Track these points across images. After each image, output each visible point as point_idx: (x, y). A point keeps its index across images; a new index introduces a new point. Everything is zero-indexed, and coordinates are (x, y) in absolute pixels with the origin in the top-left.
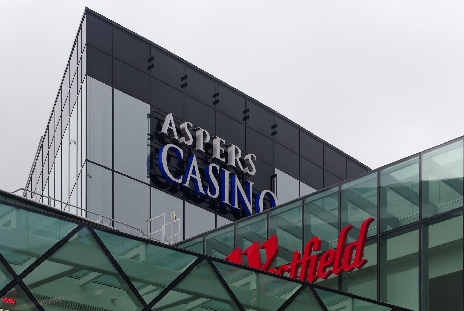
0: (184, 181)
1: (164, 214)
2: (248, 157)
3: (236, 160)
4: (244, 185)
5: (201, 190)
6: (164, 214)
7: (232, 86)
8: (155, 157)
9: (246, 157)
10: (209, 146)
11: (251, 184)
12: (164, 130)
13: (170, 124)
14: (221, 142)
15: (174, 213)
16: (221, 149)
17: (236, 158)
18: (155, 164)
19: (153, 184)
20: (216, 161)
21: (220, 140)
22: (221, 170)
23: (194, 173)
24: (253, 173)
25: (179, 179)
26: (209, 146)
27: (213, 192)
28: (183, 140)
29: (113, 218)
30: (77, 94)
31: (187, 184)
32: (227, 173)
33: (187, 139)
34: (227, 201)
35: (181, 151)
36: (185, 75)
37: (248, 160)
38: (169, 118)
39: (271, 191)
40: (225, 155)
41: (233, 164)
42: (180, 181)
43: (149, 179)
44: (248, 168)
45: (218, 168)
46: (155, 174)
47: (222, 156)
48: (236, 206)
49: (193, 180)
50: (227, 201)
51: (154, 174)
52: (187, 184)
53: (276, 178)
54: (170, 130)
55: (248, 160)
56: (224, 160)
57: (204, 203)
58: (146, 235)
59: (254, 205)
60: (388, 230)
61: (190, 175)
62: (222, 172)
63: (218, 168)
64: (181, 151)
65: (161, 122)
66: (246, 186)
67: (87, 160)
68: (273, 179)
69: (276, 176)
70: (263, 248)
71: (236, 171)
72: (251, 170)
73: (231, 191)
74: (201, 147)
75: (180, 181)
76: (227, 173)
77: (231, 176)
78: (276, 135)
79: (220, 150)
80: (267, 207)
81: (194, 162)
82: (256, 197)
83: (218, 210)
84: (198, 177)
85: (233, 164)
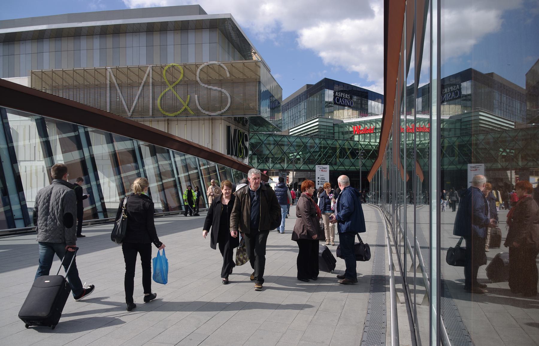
2: (348, 95)
10: (342, 96)
12: (336, 95)
38: (337, 93)
49: (340, 102)
66: (348, 101)
77: (346, 100)
82: (350, 102)
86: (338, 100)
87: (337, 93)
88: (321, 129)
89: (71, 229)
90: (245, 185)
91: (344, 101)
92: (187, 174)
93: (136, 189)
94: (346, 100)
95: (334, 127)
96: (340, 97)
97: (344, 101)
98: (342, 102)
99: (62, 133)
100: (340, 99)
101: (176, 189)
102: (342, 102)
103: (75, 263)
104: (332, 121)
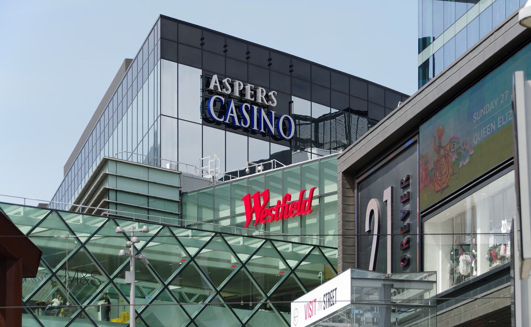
0: (225, 119)
1: (209, 157)
2: (271, 93)
3: (262, 98)
4: (269, 116)
5: (237, 123)
6: (209, 157)
7: (259, 44)
8: (206, 105)
9: (269, 94)
10: (242, 93)
11: (273, 112)
12: (212, 87)
13: (216, 82)
14: (251, 87)
15: (216, 155)
16: (251, 92)
17: (262, 96)
18: (205, 109)
19: (205, 122)
20: (247, 101)
21: (251, 86)
22: (251, 107)
23: (232, 112)
24: (275, 105)
25: (222, 118)
26: (242, 93)
27: (245, 123)
28: (224, 91)
29: (178, 161)
30: (154, 66)
31: (227, 121)
32: (256, 108)
33: (227, 90)
34: (255, 128)
35: (223, 99)
36: (226, 44)
37: (271, 95)
38: (215, 78)
39: (289, 115)
40: (254, 95)
41: (260, 101)
42: (222, 120)
43: (201, 119)
44: (271, 102)
45: (249, 106)
46: (206, 117)
47: (252, 97)
48: (262, 130)
49: (233, 118)
50: (255, 128)
51: (204, 117)
52: (227, 121)
53: (292, 104)
54: (216, 87)
55: (271, 95)
56: (253, 99)
57: (240, 129)
58: (198, 169)
59: (276, 128)
60: (325, 193)
61: (229, 114)
62: (252, 108)
63: (249, 106)
64: (223, 99)
65: (210, 79)
66: (269, 114)
67: (161, 115)
68: (290, 104)
69: (292, 102)
70: (262, 195)
71: (261, 106)
72: (273, 102)
73: (258, 117)
74: (237, 94)
75: (222, 120)
76: (256, 108)
77: (259, 112)
78: (292, 73)
79: (251, 93)
80: (287, 126)
81: (232, 105)
82: (277, 118)
83: (251, 132)
84: (235, 115)
85: (260, 101)
86: (223, 111)
87: (215, 78)
88: (151, 200)
89: (36, 278)
90: (108, 295)
91: (250, 112)
92: (67, 250)
93: (236, 265)
94: (259, 112)
95: (181, 204)
96: (229, 97)
97: (250, 112)
98: (241, 117)
99: (491, 270)
100: (229, 104)
101: (412, 281)
102: (241, 117)
103: (445, 295)
104: (175, 181)
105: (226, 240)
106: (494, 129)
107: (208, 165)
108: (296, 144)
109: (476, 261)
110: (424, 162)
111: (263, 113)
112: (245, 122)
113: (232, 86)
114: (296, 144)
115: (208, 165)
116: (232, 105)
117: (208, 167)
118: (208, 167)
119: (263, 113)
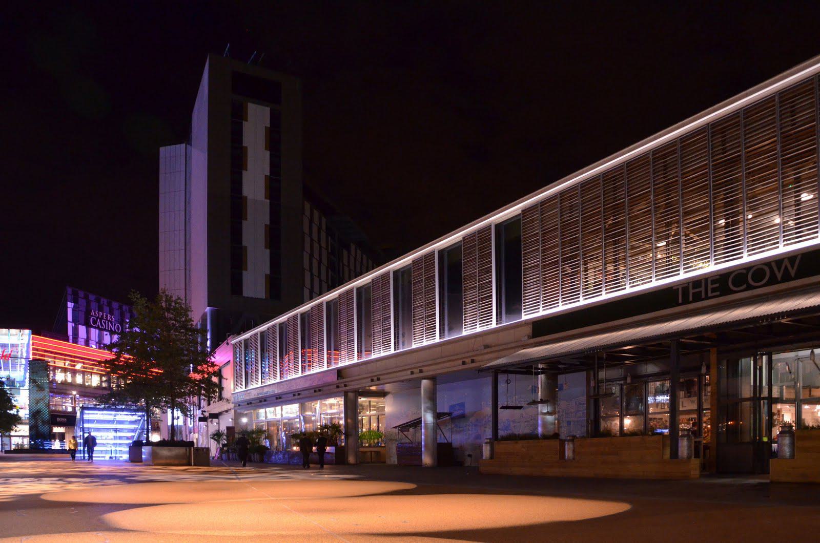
10: (102, 316)
26: (102, 316)
71: (109, 321)
77: (108, 323)
81: (99, 320)
82: (115, 325)
84: (99, 324)
94: (108, 323)
100: (97, 320)
105: (749, 397)
106: (49, 364)
107: (701, 287)
108: (101, 337)
109: (108, 444)
110: (360, 391)
111: (110, 324)
112: (103, 327)
113: (99, 314)
114: (101, 337)
115: (701, 287)
116: (99, 320)
117: (701, 291)
118: (701, 291)
119: (110, 324)
